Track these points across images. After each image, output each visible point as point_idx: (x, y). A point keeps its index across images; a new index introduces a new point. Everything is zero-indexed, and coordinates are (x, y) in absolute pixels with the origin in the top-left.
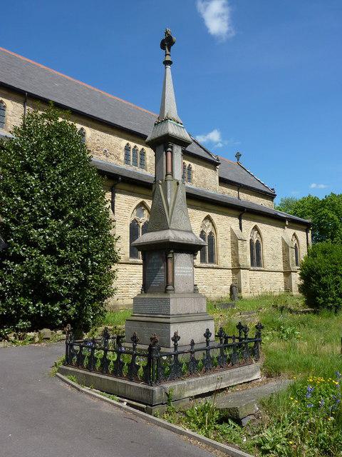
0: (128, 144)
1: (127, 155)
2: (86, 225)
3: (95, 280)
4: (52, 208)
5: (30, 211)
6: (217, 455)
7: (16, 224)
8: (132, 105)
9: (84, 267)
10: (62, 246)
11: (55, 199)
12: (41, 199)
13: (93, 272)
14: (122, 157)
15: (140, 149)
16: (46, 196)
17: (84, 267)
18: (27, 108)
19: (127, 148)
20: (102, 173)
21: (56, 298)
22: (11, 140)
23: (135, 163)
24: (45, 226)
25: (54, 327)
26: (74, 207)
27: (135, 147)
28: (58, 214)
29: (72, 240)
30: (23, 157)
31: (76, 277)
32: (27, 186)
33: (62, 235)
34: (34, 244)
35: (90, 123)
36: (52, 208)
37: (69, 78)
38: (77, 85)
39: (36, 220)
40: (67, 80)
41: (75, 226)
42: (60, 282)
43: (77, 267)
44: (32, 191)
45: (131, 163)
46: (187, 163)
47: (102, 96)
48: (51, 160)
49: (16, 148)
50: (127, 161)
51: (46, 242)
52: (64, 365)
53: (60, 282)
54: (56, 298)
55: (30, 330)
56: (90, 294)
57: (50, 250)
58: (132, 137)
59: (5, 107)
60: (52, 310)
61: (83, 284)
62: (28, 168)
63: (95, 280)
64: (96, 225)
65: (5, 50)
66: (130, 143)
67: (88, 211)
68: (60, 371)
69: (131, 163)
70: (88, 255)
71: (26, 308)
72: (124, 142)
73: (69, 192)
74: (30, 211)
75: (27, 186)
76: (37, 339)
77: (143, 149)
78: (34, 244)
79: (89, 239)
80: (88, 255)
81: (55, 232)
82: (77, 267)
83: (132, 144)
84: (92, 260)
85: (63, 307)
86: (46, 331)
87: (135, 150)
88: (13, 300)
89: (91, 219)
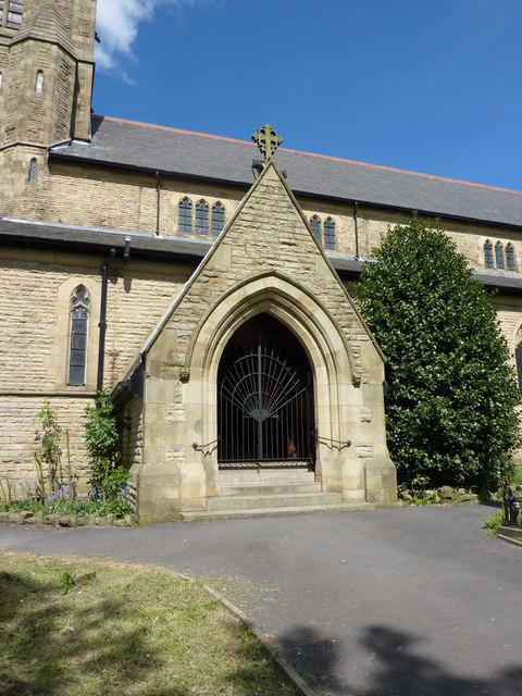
0: (487, 241)
1: (488, 256)
2: (481, 358)
3: (500, 425)
4: (436, 339)
5: (414, 346)
6: (262, 693)
7: (398, 362)
8: (483, 186)
9: (484, 409)
10: (457, 384)
11: (441, 327)
12: (423, 330)
13: (496, 415)
14: (482, 260)
15: (505, 245)
16: (430, 327)
17: (484, 409)
18: (358, 219)
19: (487, 247)
20: (489, 288)
21: (455, 448)
22: (372, 266)
23: (202, 227)
24: (431, 362)
25: (455, 484)
26: (463, 336)
27: (498, 242)
28: (447, 347)
29: (467, 377)
30: (394, 283)
31: (478, 422)
32: (404, 317)
33: (457, 370)
34: (421, 384)
35: (231, 192)
36: (436, 339)
37: (395, 170)
38: (408, 177)
39: (421, 356)
40: (395, 173)
41: (468, 359)
42: (458, 429)
43: (477, 409)
44: (411, 322)
45: (495, 265)
46: (309, 214)
47: (440, 183)
48: (431, 282)
49: (385, 275)
50: (489, 263)
51: (436, 380)
52: (504, 524)
53: (458, 429)
54: (455, 448)
55: (428, 487)
56: (495, 443)
57: (443, 390)
58: (491, 231)
59: (223, 209)
60: (453, 463)
61: (486, 431)
62: (401, 295)
63: (500, 425)
64: (493, 355)
65: (227, 139)
66: (491, 239)
67: (482, 338)
68: (500, 531)
69: (495, 265)
70: (488, 394)
71: (422, 461)
72: (482, 240)
73: (457, 319)
74: (414, 346)
75: (404, 317)
76: (438, 499)
77: (509, 244)
78: (421, 384)
79: (486, 373)
80: (488, 394)
81: (445, 368)
82: (477, 409)
83: (494, 240)
84: (495, 400)
85: (465, 460)
86: (446, 489)
87: (498, 247)
88: (406, 452)
89: (486, 348)
